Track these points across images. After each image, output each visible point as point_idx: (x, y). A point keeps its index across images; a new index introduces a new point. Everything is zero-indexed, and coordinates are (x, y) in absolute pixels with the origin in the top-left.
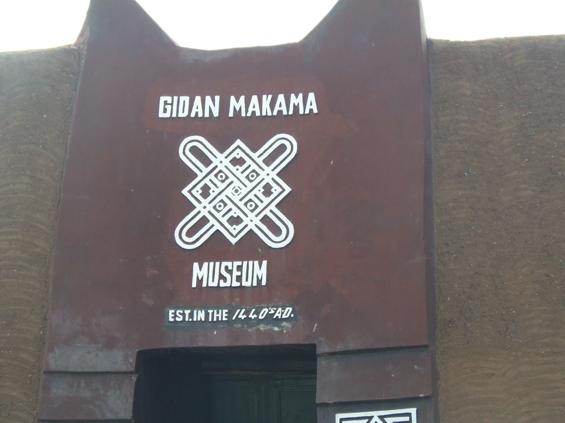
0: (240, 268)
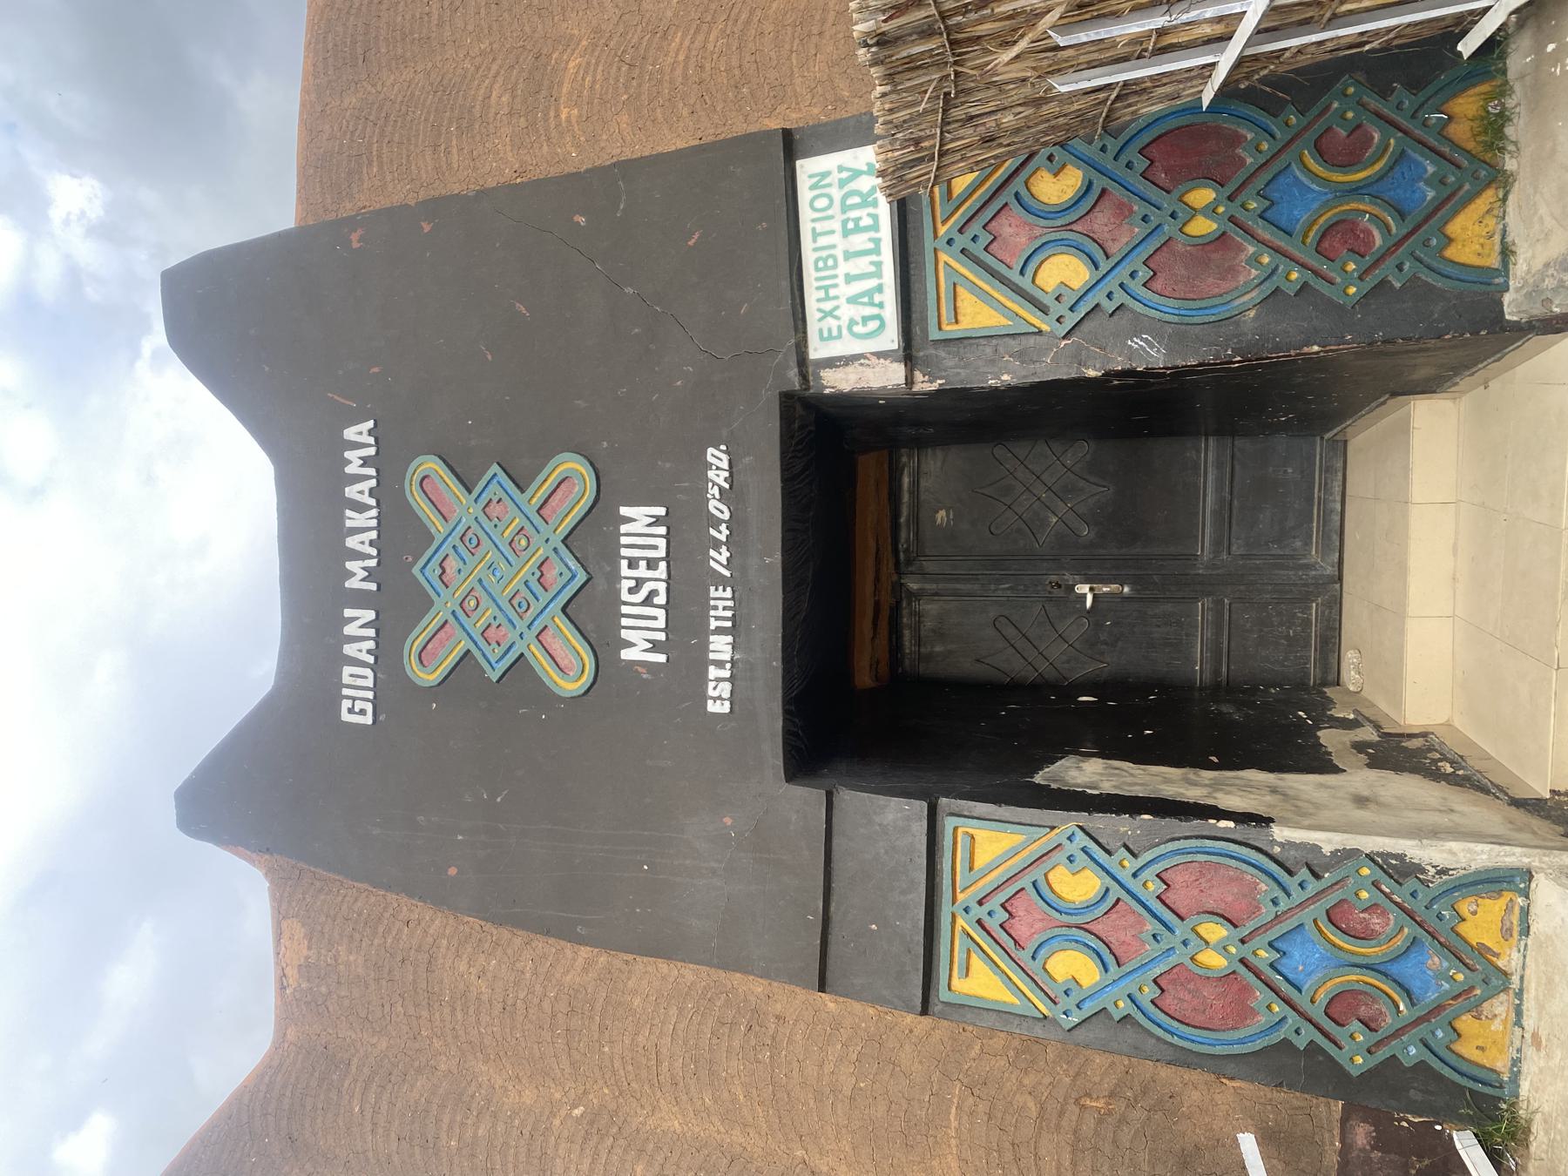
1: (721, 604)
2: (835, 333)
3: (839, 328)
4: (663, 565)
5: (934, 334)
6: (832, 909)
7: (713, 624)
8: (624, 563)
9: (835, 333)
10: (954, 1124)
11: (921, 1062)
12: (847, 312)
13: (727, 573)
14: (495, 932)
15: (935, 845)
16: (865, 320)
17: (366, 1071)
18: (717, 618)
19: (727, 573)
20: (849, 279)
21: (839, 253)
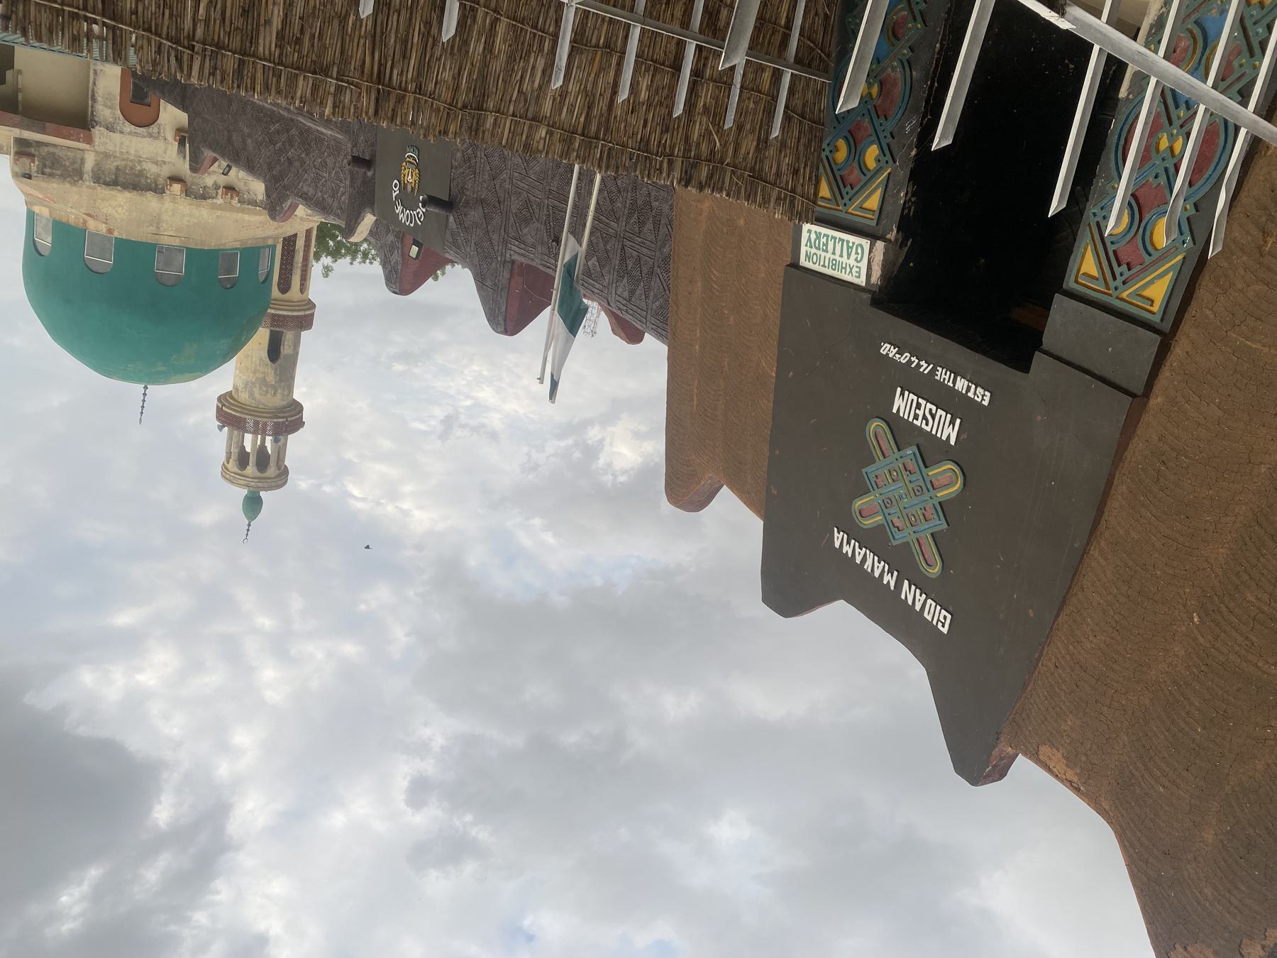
0: (916, 417)
1: (943, 376)
2: (858, 270)
3: (857, 267)
4: (920, 400)
5: (873, 223)
6: (1097, 372)
7: (951, 384)
8: (915, 422)
9: (858, 270)
10: (1258, 346)
11: (1210, 354)
12: (852, 262)
13: (931, 366)
14: (1071, 608)
15: (1073, 294)
16: (857, 253)
17: (1139, 765)
18: (949, 381)
19: (931, 366)
20: (841, 256)
21: (832, 257)
